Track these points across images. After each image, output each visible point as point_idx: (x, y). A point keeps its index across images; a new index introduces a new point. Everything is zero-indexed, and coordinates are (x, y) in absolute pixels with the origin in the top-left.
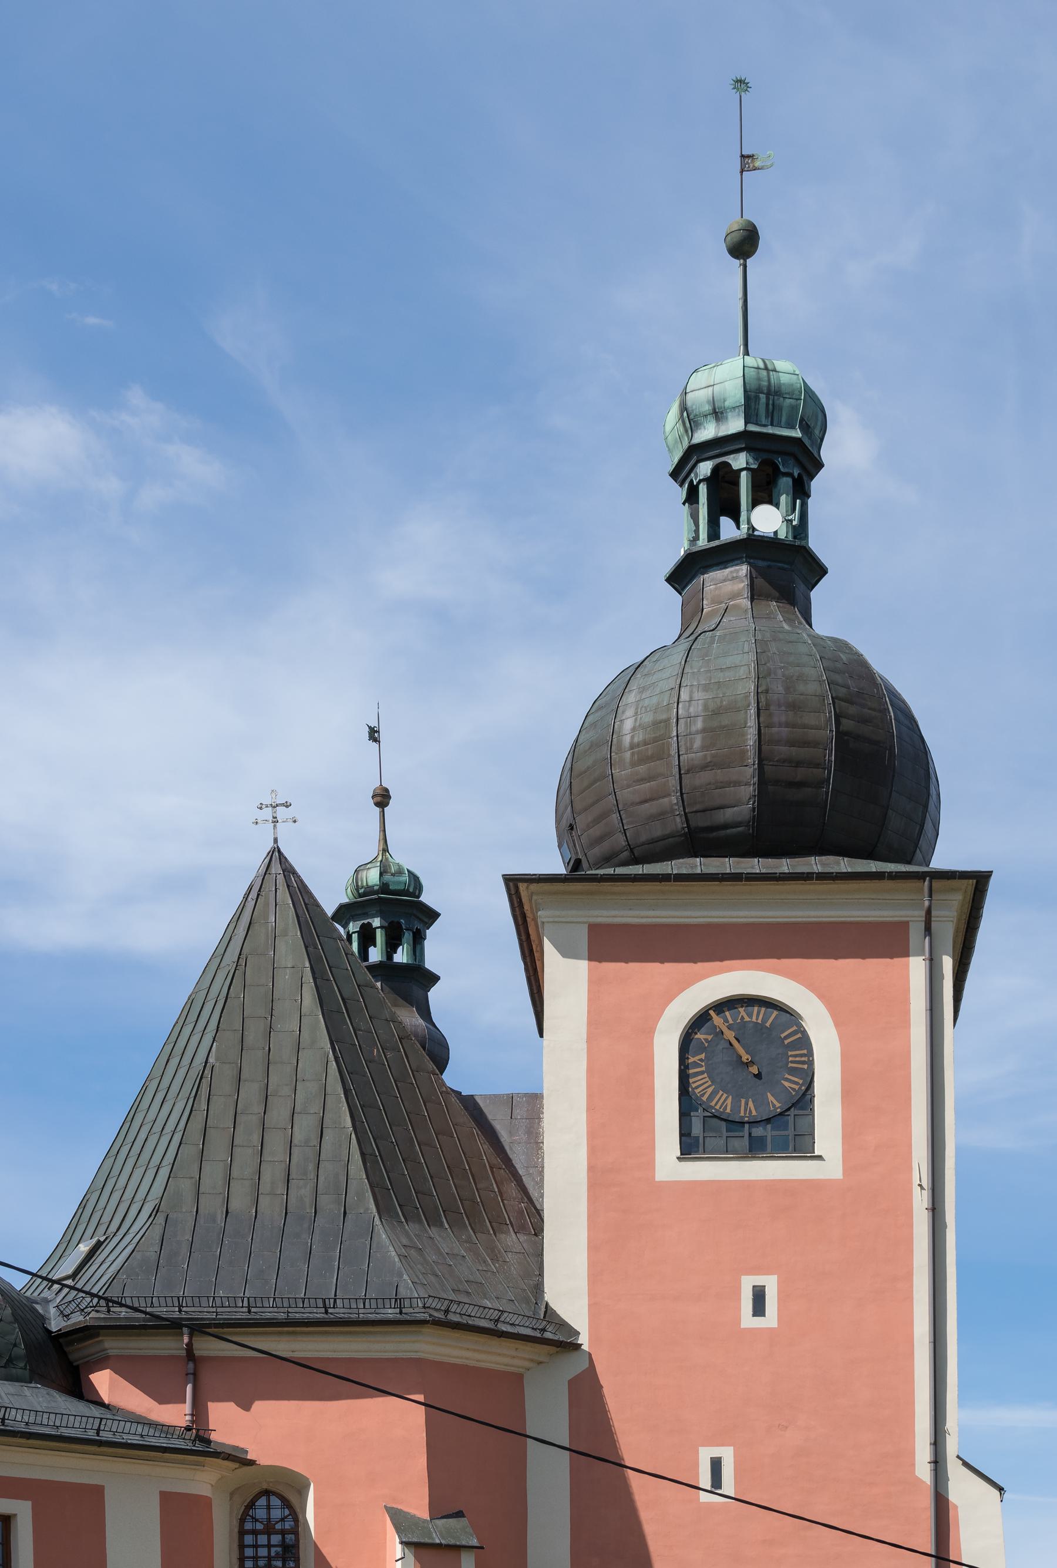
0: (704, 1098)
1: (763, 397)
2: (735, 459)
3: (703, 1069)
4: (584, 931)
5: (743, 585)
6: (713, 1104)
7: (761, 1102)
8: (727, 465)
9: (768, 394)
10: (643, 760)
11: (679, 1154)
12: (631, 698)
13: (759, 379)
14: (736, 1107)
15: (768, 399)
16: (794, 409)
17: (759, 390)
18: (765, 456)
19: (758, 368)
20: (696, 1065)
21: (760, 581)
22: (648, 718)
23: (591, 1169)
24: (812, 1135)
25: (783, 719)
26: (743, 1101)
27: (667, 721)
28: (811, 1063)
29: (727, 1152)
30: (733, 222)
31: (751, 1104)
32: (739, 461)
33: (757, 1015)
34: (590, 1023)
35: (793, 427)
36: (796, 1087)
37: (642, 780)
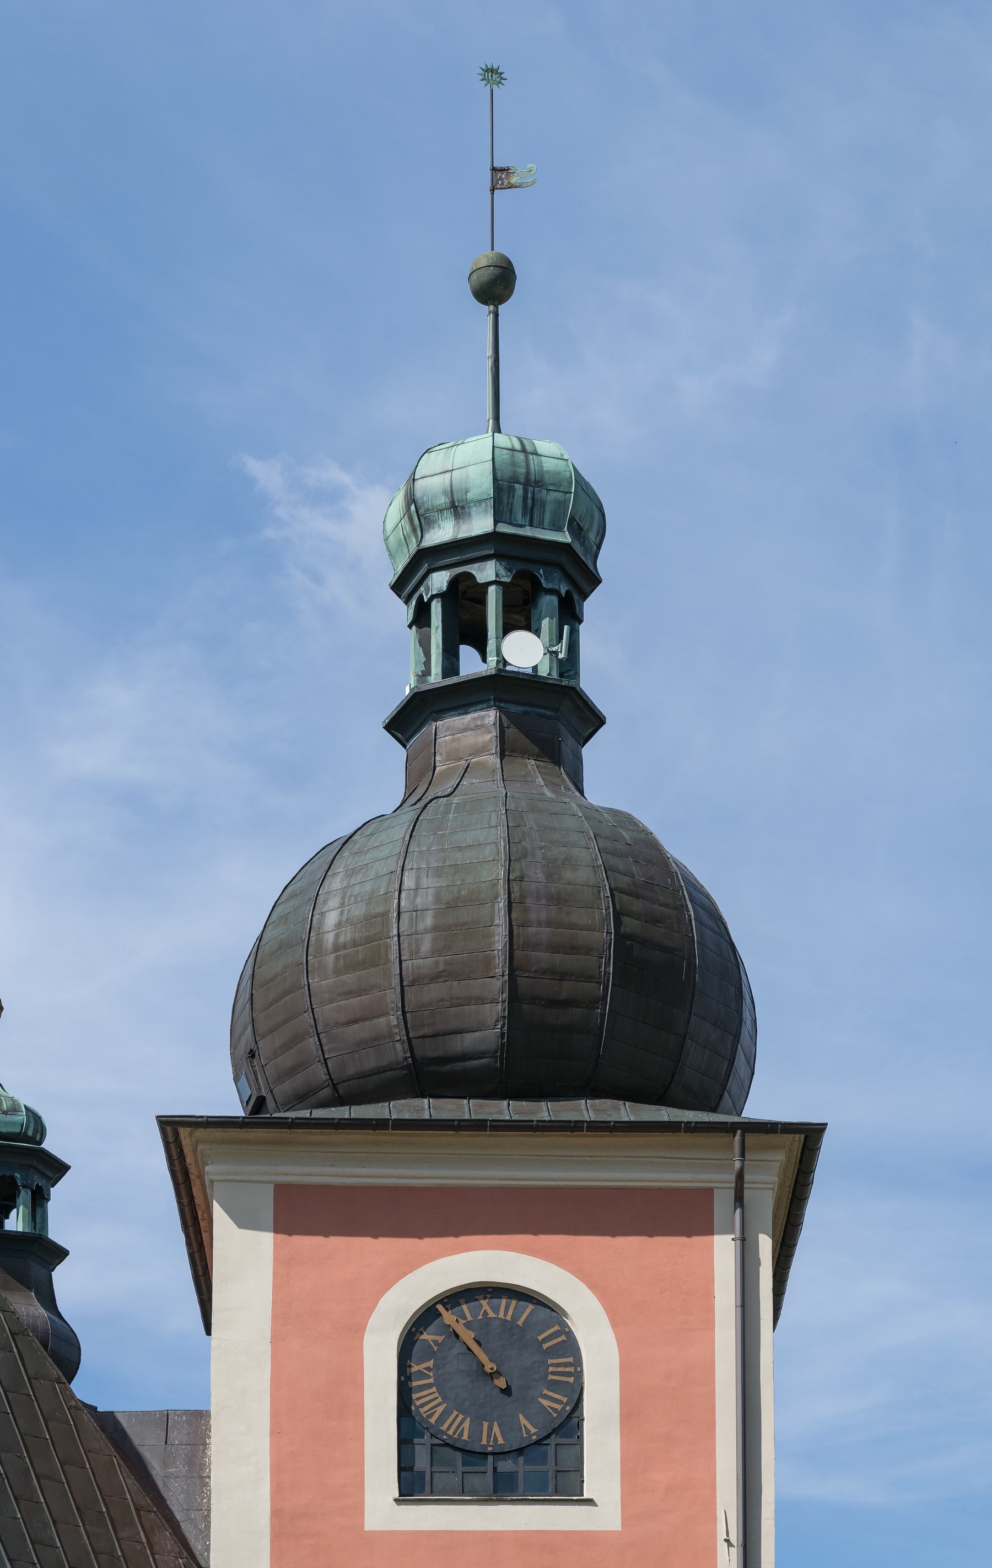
0: (433, 1421)
1: (519, 489)
2: (481, 570)
3: (431, 1381)
4: (270, 1190)
5: (489, 737)
6: (444, 1428)
7: (510, 1427)
8: (470, 577)
9: (526, 484)
10: (353, 966)
11: (397, 1495)
12: (335, 883)
13: (514, 464)
14: (476, 1432)
15: (526, 491)
16: (562, 504)
17: (514, 479)
18: (520, 566)
19: (513, 450)
20: (421, 1375)
21: (512, 732)
22: (358, 911)
23: (276, 1513)
24: (580, 1470)
25: (543, 916)
26: (486, 1425)
27: (385, 915)
28: (579, 1375)
29: (463, 1493)
30: (482, 256)
31: (496, 1429)
32: (486, 572)
33: (505, 1309)
34: (275, 1317)
35: (559, 529)
36: (559, 1407)
37: (349, 993)
